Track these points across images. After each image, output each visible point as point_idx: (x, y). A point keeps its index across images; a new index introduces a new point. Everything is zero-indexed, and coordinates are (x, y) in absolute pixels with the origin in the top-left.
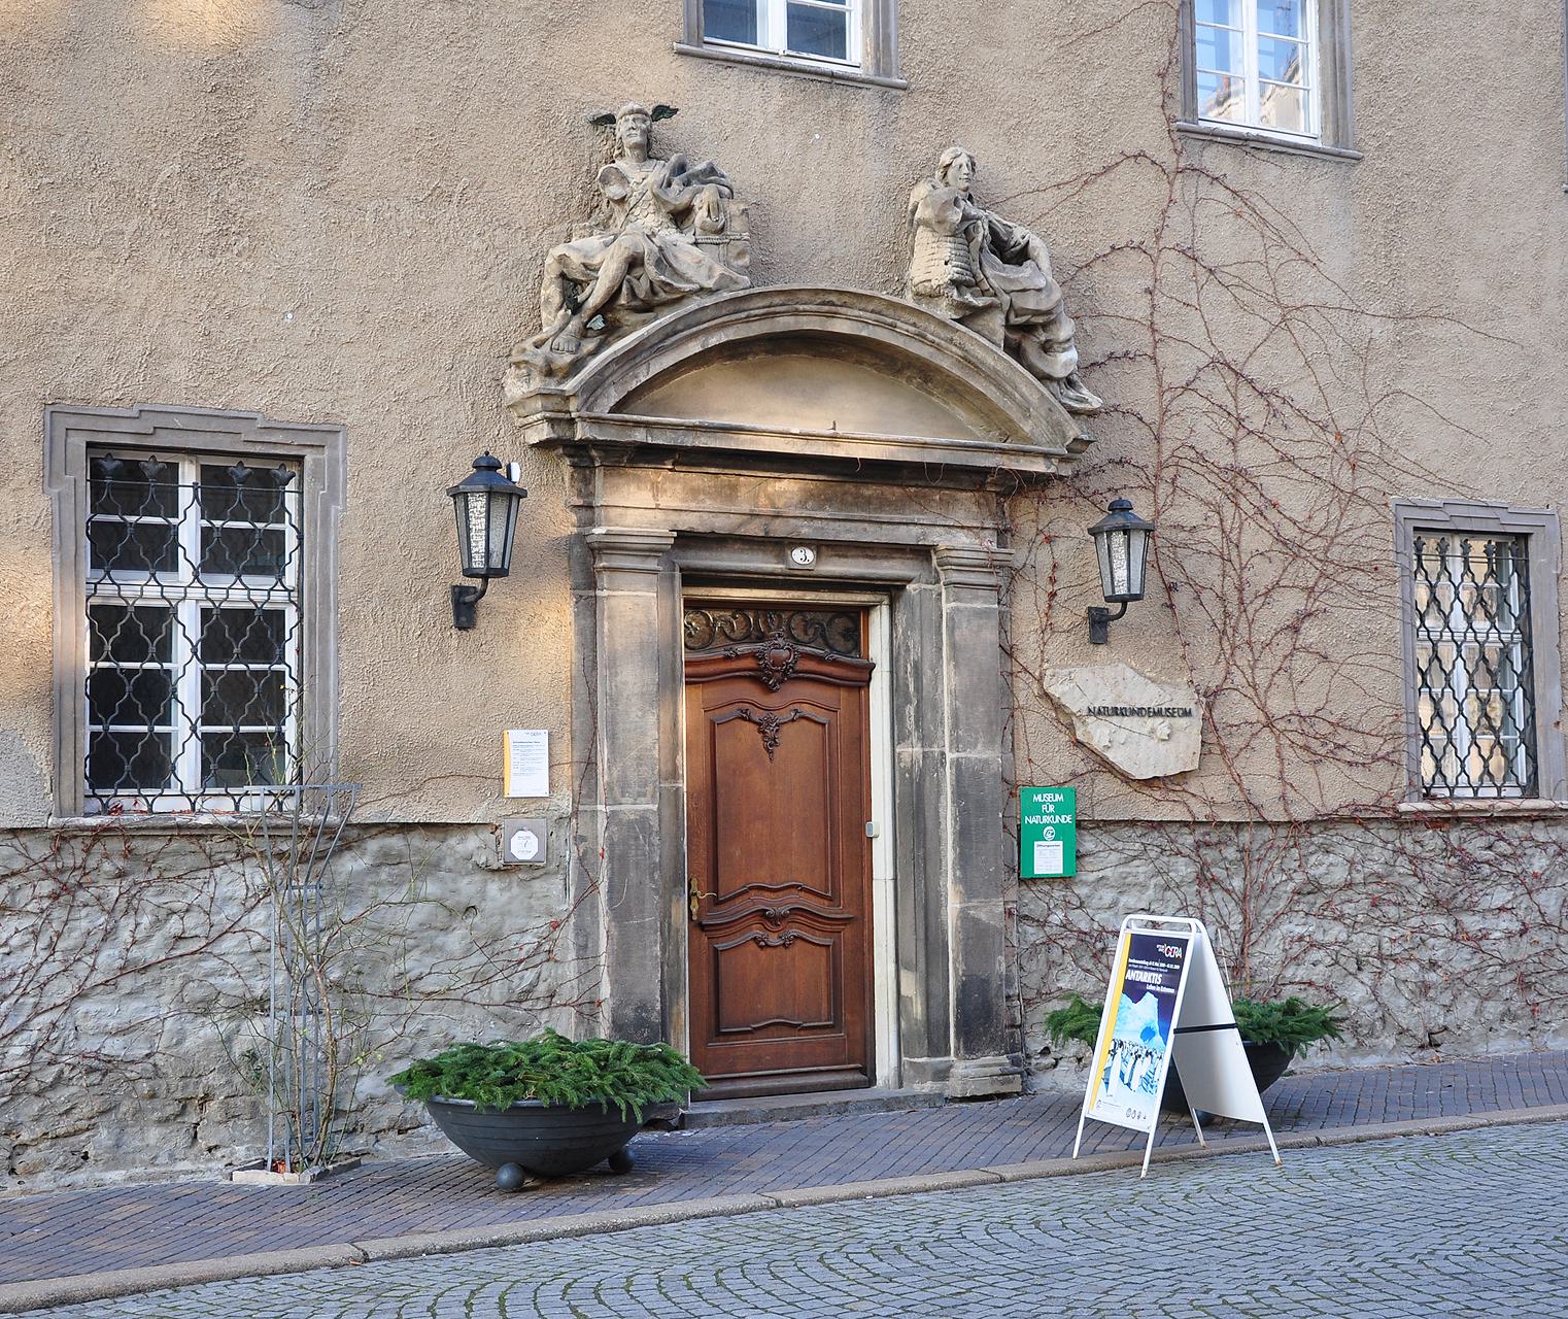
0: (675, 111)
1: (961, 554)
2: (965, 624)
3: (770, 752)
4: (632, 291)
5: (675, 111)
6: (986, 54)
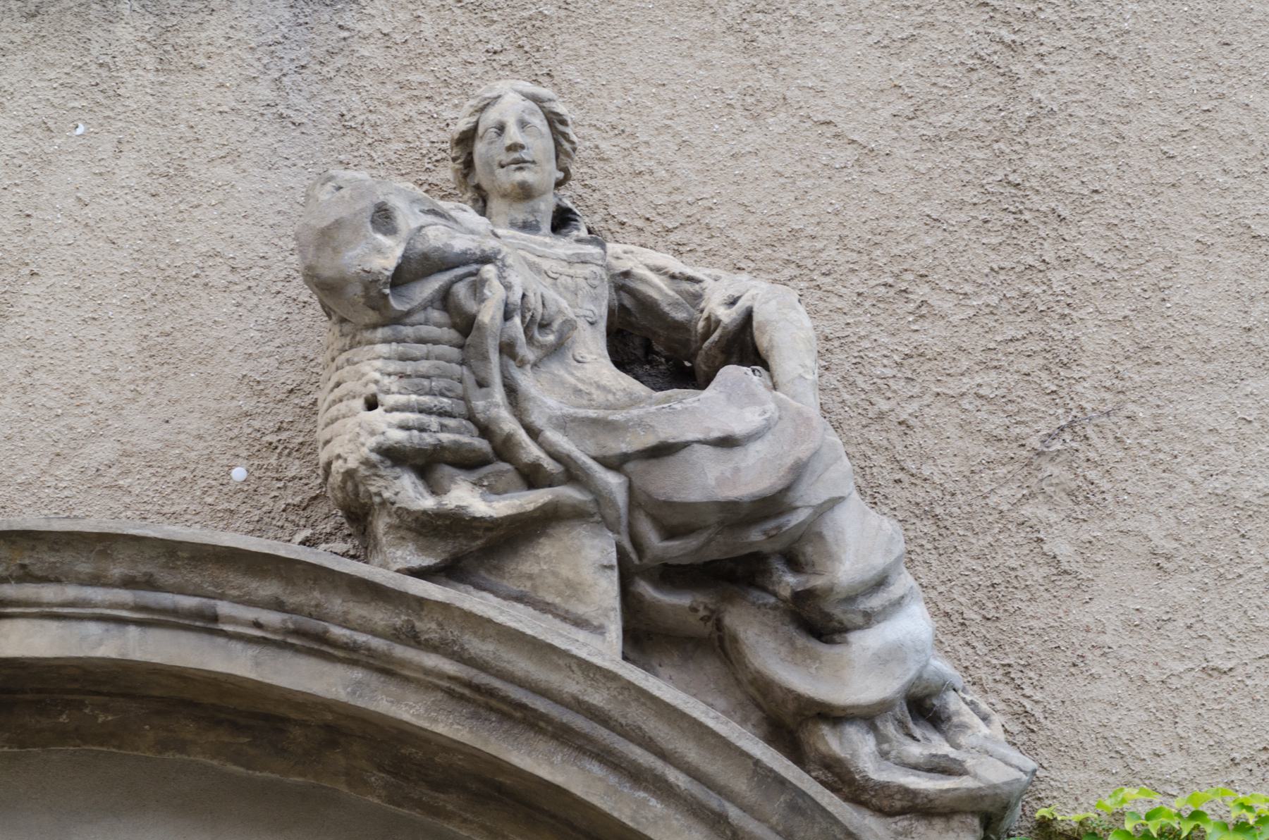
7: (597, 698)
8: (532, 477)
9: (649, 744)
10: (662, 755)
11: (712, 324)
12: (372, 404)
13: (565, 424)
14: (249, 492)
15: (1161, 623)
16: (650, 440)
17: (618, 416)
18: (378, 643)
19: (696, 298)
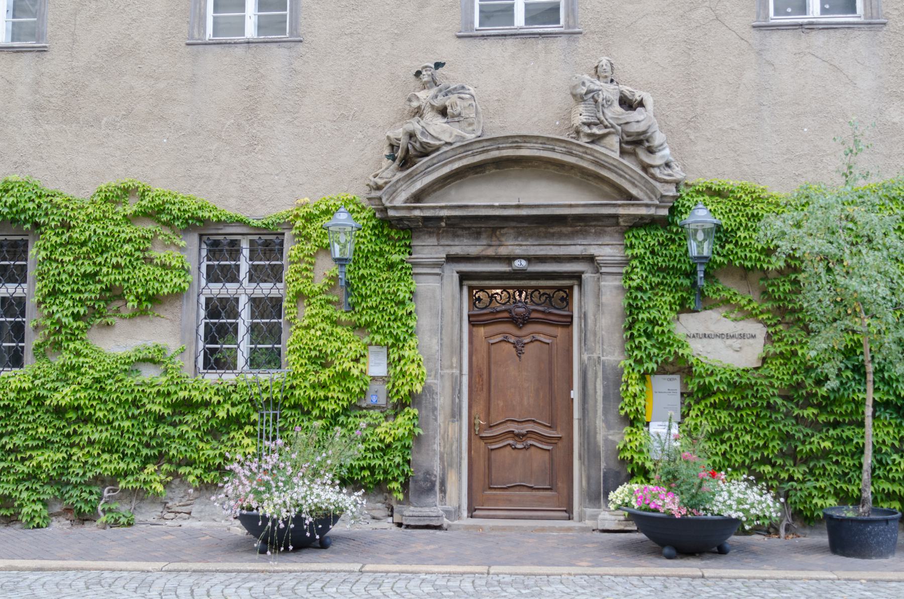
0: (444, 64)
1: (605, 258)
2: (608, 293)
4: (414, 147)
5: (444, 64)
7: (615, 163)
8: (606, 127)
9: (623, 171)
10: (625, 173)
11: (636, 100)
13: (611, 118)
14: (559, 126)
15: (708, 150)
16: (625, 121)
17: (620, 117)
18: (581, 154)
19: (634, 95)
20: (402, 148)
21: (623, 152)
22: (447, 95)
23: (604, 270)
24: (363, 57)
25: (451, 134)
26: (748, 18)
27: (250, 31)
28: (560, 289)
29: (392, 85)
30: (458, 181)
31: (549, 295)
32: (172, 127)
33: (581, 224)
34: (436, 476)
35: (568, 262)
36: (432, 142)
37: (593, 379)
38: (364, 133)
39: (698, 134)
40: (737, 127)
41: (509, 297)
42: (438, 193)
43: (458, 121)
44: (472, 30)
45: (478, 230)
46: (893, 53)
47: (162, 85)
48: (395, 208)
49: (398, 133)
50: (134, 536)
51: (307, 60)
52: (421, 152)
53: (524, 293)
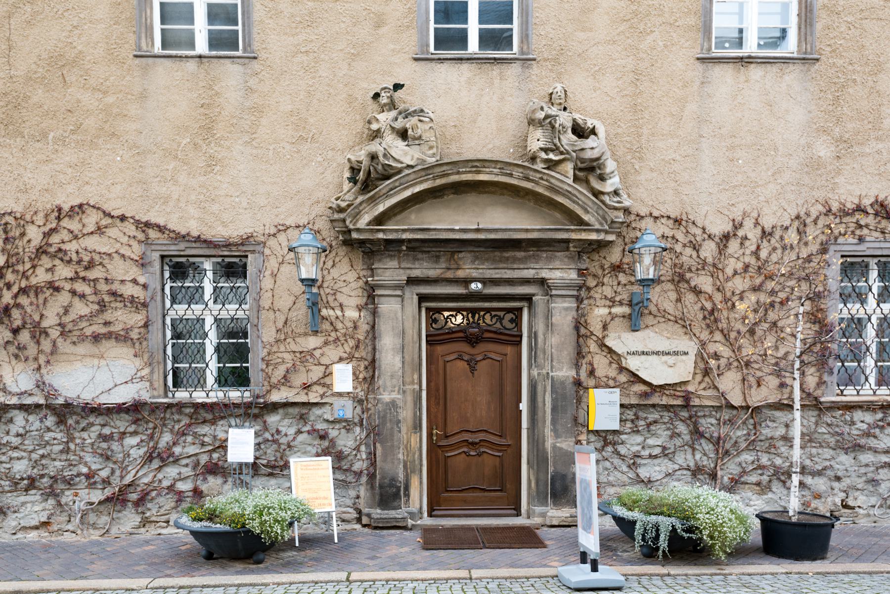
0: (403, 86)
1: (556, 281)
2: (558, 314)
3: (473, 373)
4: (375, 169)
5: (403, 86)
6: (581, 35)
7: (570, 189)
8: (562, 153)
9: (577, 197)
11: (589, 128)
12: (538, 140)
13: (567, 145)
14: (513, 153)
15: (651, 180)
16: (580, 148)
20: (365, 170)
21: (576, 179)
22: (407, 117)
23: (554, 292)
24: (320, 77)
25: (413, 156)
26: (693, 50)
27: (202, 46)
28: (509, 310)
29: (350, 107)
30: (417, 206)
31: (500, 316)
32: (126, 145)
33: (534, 249)
34: (401, 482)
35: (520, 285)
36: (394, 164)
37: (542, 393)
38: (323, 156)
39: (642, 164)
40: (678, 158)
41: (463, 319)
42: (399, 217)
43: (419, 145)
44: (428, 52)
45: (438, 254)
46: (823, 88)
47: (110, 99)
48: (358, 230)
49: (361, 155)
50: (115, 548)
51: (263, 78)
52: (383, 175)
53: (477, 316)
